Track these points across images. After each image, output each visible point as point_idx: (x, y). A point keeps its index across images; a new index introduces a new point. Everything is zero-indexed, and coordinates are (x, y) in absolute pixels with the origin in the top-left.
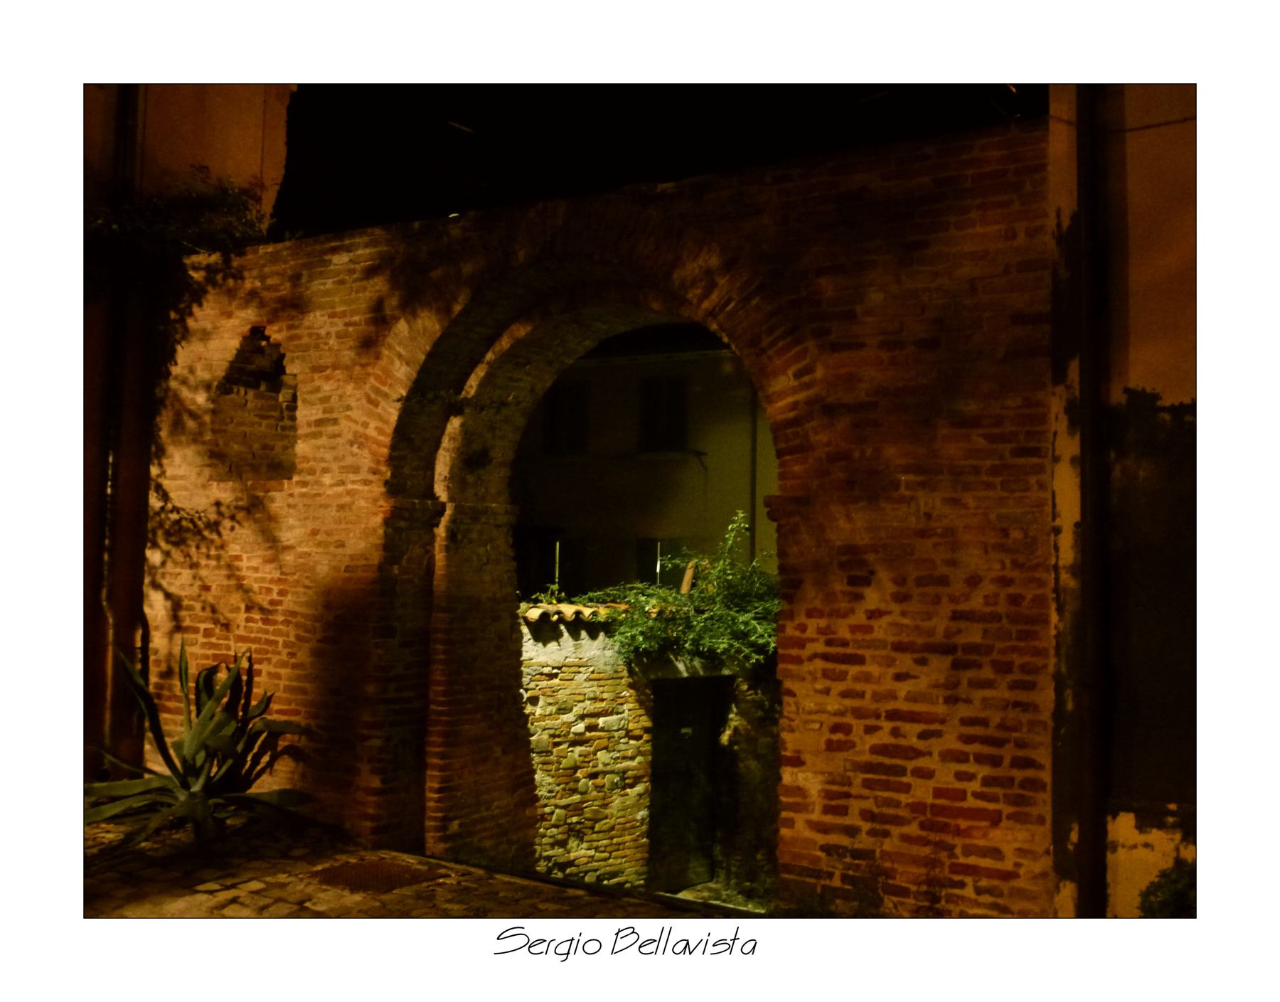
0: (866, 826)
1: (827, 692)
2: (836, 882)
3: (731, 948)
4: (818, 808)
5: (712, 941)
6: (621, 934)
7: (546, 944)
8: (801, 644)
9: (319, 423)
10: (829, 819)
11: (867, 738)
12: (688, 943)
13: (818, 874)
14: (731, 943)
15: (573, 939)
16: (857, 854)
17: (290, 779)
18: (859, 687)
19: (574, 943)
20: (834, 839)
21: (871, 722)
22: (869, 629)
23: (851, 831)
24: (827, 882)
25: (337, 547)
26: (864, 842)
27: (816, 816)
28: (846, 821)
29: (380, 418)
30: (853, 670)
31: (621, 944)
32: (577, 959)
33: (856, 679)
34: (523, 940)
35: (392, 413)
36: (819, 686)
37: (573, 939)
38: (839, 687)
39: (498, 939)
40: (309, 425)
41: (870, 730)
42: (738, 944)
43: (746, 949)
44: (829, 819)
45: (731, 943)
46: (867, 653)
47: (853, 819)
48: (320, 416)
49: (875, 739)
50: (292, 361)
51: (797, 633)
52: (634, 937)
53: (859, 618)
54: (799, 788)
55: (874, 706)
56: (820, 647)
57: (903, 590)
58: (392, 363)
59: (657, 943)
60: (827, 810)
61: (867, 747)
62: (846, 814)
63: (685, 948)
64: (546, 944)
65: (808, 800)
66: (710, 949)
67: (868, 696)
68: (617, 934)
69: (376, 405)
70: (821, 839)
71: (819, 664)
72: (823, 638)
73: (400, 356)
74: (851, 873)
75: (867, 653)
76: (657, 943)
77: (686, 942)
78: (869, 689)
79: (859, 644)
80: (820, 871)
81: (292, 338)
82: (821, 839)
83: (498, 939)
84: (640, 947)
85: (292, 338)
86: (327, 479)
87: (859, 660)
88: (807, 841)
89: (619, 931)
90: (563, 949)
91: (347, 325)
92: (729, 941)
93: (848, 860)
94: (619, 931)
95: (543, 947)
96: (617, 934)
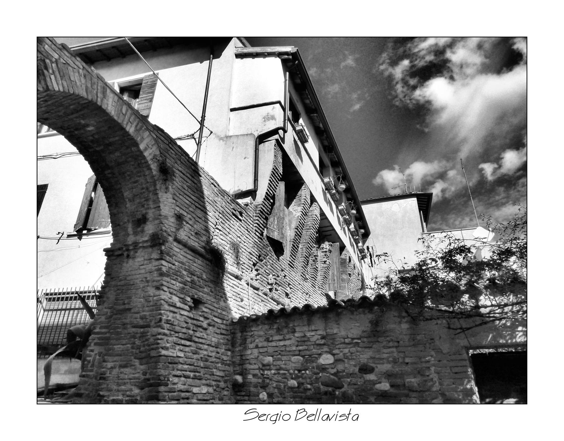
3: (348, 418)
6: (299, 412)
7: (266, 416)
15: (278, 414)
19: (279, 416)
31: (299, 416)
32: (280, 423)
34: (256, 414)
37: (278, 414)
42: (351, 416)
43: (355, 418)
45: (347, 416)
52: (305, 413)
64: (266, 416)
66: (338, 418)
68: (297, 412)
90: (274, 418)
92: (346, 415)
95: (265, 417)
96: (297, 412)
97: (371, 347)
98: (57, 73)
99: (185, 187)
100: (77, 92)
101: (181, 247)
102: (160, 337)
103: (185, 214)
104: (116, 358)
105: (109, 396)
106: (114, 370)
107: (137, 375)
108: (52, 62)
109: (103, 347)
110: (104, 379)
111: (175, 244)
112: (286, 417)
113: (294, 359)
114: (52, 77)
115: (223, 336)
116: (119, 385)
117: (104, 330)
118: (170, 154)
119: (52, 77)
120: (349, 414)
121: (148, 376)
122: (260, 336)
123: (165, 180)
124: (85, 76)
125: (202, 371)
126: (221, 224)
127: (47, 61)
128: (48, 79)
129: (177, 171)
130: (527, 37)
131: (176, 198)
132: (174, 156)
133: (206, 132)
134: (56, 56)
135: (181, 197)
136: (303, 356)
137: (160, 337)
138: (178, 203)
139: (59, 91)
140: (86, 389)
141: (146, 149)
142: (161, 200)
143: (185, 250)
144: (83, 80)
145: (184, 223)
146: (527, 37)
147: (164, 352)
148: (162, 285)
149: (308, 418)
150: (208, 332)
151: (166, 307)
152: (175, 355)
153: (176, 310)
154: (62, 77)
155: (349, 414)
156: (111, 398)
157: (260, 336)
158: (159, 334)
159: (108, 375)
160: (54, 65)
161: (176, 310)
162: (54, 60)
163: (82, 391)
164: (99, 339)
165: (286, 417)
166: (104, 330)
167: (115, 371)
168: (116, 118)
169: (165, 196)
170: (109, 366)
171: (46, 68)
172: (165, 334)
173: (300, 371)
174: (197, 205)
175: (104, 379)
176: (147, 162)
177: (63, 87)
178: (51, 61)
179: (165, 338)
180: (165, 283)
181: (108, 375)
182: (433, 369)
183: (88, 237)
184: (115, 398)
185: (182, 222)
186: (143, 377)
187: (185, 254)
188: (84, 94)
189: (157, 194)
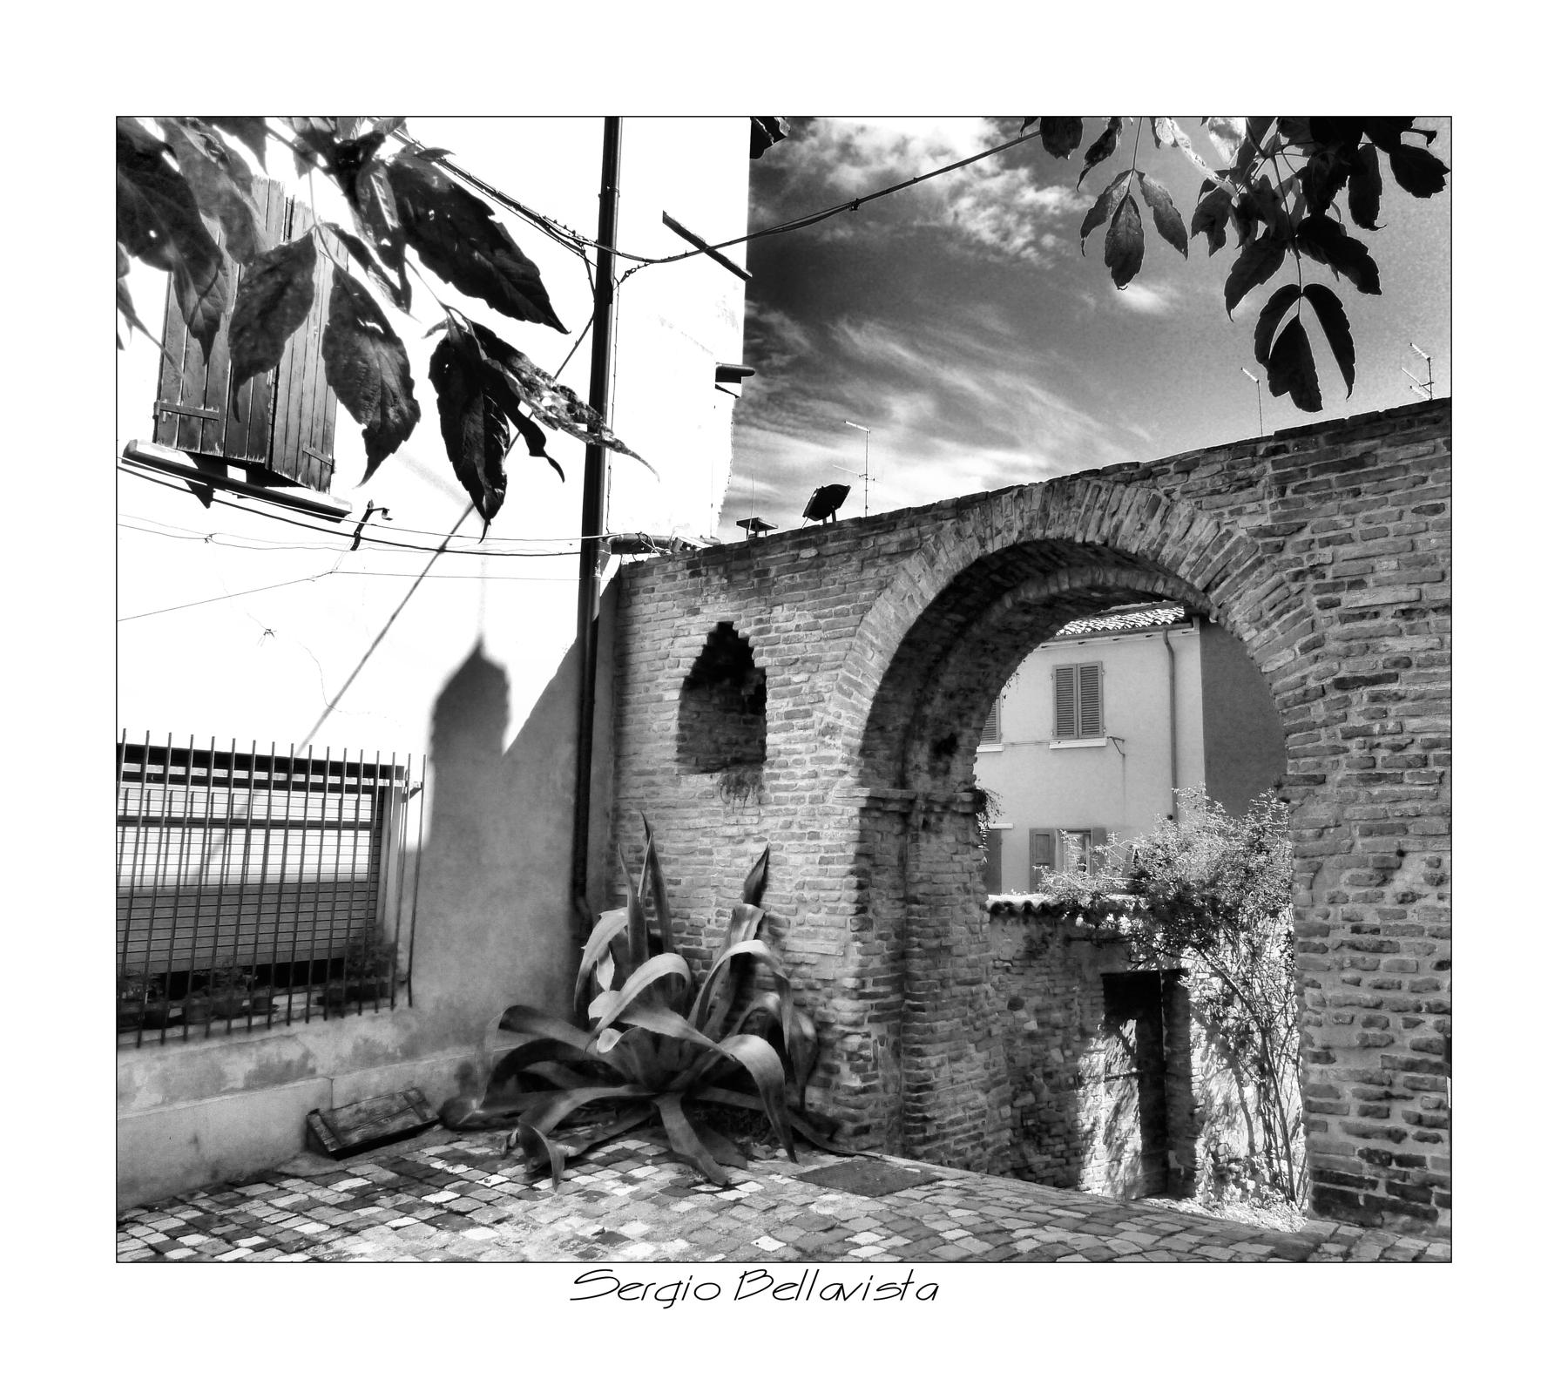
0: (1413, 1130)
1: (1357, 983)
2: (1381, 1192)
3: (902, 1293)
4: (1354, 1110)
5: (875, 1285)
6: (747, 1278)
7: (643, 1288)
8: (1325, 931)
9: (789, 715)
10: (1368, 1122)
11: (1407, 1032)
12: (842, 1287)
13: (1360, 1182)
14: (902, 1288)
15: (680, 1283)
16: (1403, 1161)
17: (761, 1076)
18: (1396, 977)
19: (682, 1288)
20: (1374, 1144)
21: (1411, 1015)
22: (1403, 915)
23: (1397, 1136)
24: (1371, 1192)
25: (810, 839)
26: (1409, 1148)
27: (1353, 1118)
28: (1389, 1124)
29: (854, 707)
30: (1385, 959)
31: (747, 1288)
32: (684, 1306)
33: (1389, 969)
34: (612, 1284)
35: (867, 705)
36: (1348, 975)
37: (680, 1283)
38: (1369, 979)
39: (576, 1282)
40: (779, 717)
41: (1412, 1024)
42: (912, 1289)
43: (925, 1293)
44: (1368, 1122)
45: (902, 1288)
46: (1402, 941)
47: (1396, 1122)
48: (790, 708)
49: (1415, 1035)
50: (761, 654)
51: (1320, 920)
52: (767, 1281)
53: (1389, 903)
54: (1330, 1087)
55: (1413, 998)
56: (1345, 934)
57: (1439, 872)
58: (864, 651)
59: (797, 1288)
60: (1365, 1113)
61: (1407, 1043)
62: (1388, 1116)
63: (838, 1292)
64: (643, 1288)
65: (1340, 1101)
66: (872, 1293)
67: (1405, 987)
68: (743, 1277)
69: (850, 695)
70: (1362, 1144)
71: (1348, 955)
72: (1349, 926)
73: (872, 645)
74: (1397, 1181)
75: (1402, 941)
76: (797, 1288)
77: (838, 1287)
78: (1407, 980)
79: (1392, 931)
80: (1361, 1179)
81: (760, 632)
82: (1362, 1144)
83: (576, 1282)
84: (775, 1291)
85: (760, 632)
86: (799, 772)
87: (1395, 949)
88: (1344, 1149)
89: (746, 1274)
90: (668, 1293)
91: (816, 617)
92: (899, 1286)
93: (1394, 1166)
94: (746, 1274)
95: (639, 1292)
96: (743, 1277)
104: (940, 1047)
105: (942, 1117)
106: (943, 1069)
107: (977, 1072)
109: (885, 1024)
110: (929, 1088)
112: (705, 1292)
116: (955, 1092)
117: (881, 989)
120: (907, 1284)
121: (993, 1070)
122: (713, 934)
130: (1450, 1261)
140: (872, 1116)
146: (1450, 1261)
149: (776, 1294)
155: (907, 1284)
156: (948, 1118)
157: (713, 934)
159: (935, 1079)
163: (866, 1122)
164: (877, 1007)
165: (705, 1292)
166: (881, 989)
167: (945, 1071)
170: (934, 1064)
175: (929, 1088)
181: (935, 1079)
182: (1076, 1001)
183: (242, 502)
184: (953, 1117)
186: (986, 1074)
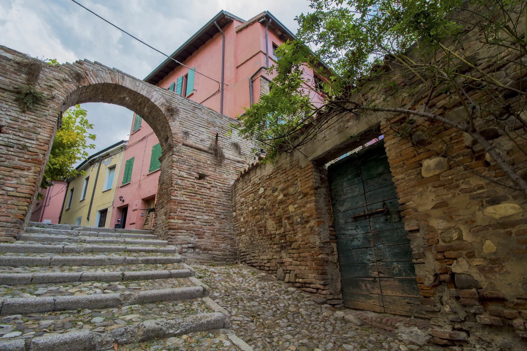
97: (276, 177)
98: (93, 76)
99: (189, 116)
100: (106, 81)
101: (188, 148)
102: (172, 191)
103: (189, 130)
108: (90, 71)
111: (184, 147)
113: (251, 195)
114: (91, 78)
115: (224, 193)
118: (174, 101)
119: (91, 78)
123: (172, 115)
124: (110, 73)
125: (205, 209)
126: (222, 134)
127: (87, 72)
128: (89, 80)
129: (181, 109)
131: (182, 123)
132: (177, 101)
133: (225, 86)
134: (92, 68)
135: (186, 122)
136: (253, 193)
137: (172, 191)
138: (184, 126)
139: (96, 84)
141: (156, 101)
142: (171, 125)
143: (192, 149)
144: (109, 75)
145: (190, 136)
147: (173, 197)
148: (173, 167)
150: (211, 190)
151: (176, 177)
152: (182, 199)
153: (184, 179)
154: (96, 77)
158: (172, 190)
160: (91, 73)
161: (184, 179)
162: (90, 70)
168: (132, 89)
169: (173, 123)
171: (87, 75)
172: (175, 190)
173: (253, 201)
174: (200, 125)
176: (158, 108)
177: (98, 81)
178: (89, 71)
179: (176, 192)
180: (174, 166)
185: (188, 135)
187: (192, 152)
188: (111, 82)
189: (168, 123)
